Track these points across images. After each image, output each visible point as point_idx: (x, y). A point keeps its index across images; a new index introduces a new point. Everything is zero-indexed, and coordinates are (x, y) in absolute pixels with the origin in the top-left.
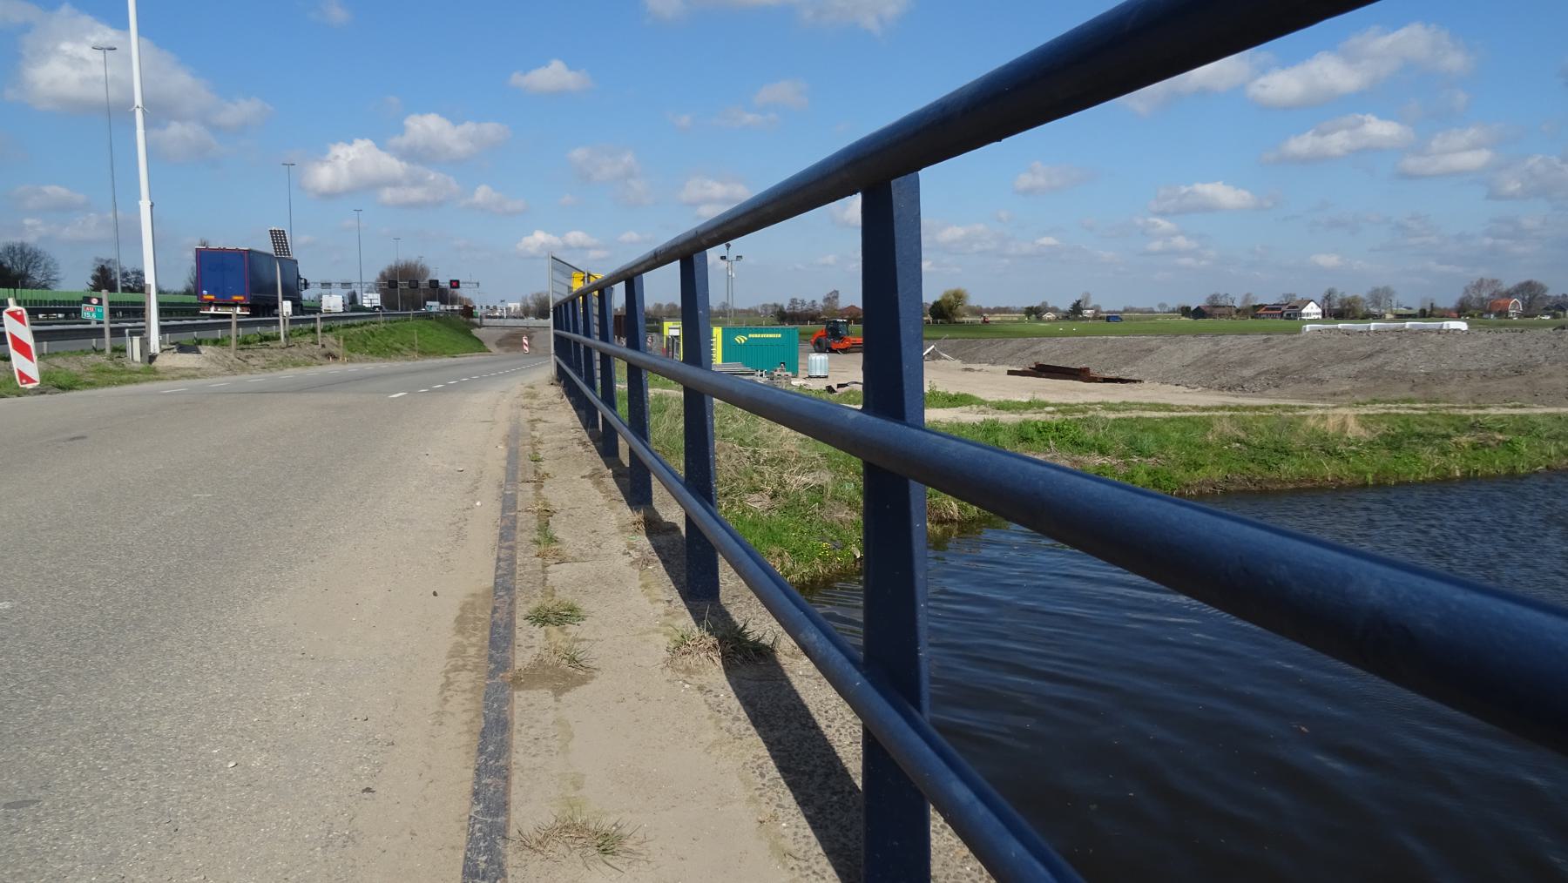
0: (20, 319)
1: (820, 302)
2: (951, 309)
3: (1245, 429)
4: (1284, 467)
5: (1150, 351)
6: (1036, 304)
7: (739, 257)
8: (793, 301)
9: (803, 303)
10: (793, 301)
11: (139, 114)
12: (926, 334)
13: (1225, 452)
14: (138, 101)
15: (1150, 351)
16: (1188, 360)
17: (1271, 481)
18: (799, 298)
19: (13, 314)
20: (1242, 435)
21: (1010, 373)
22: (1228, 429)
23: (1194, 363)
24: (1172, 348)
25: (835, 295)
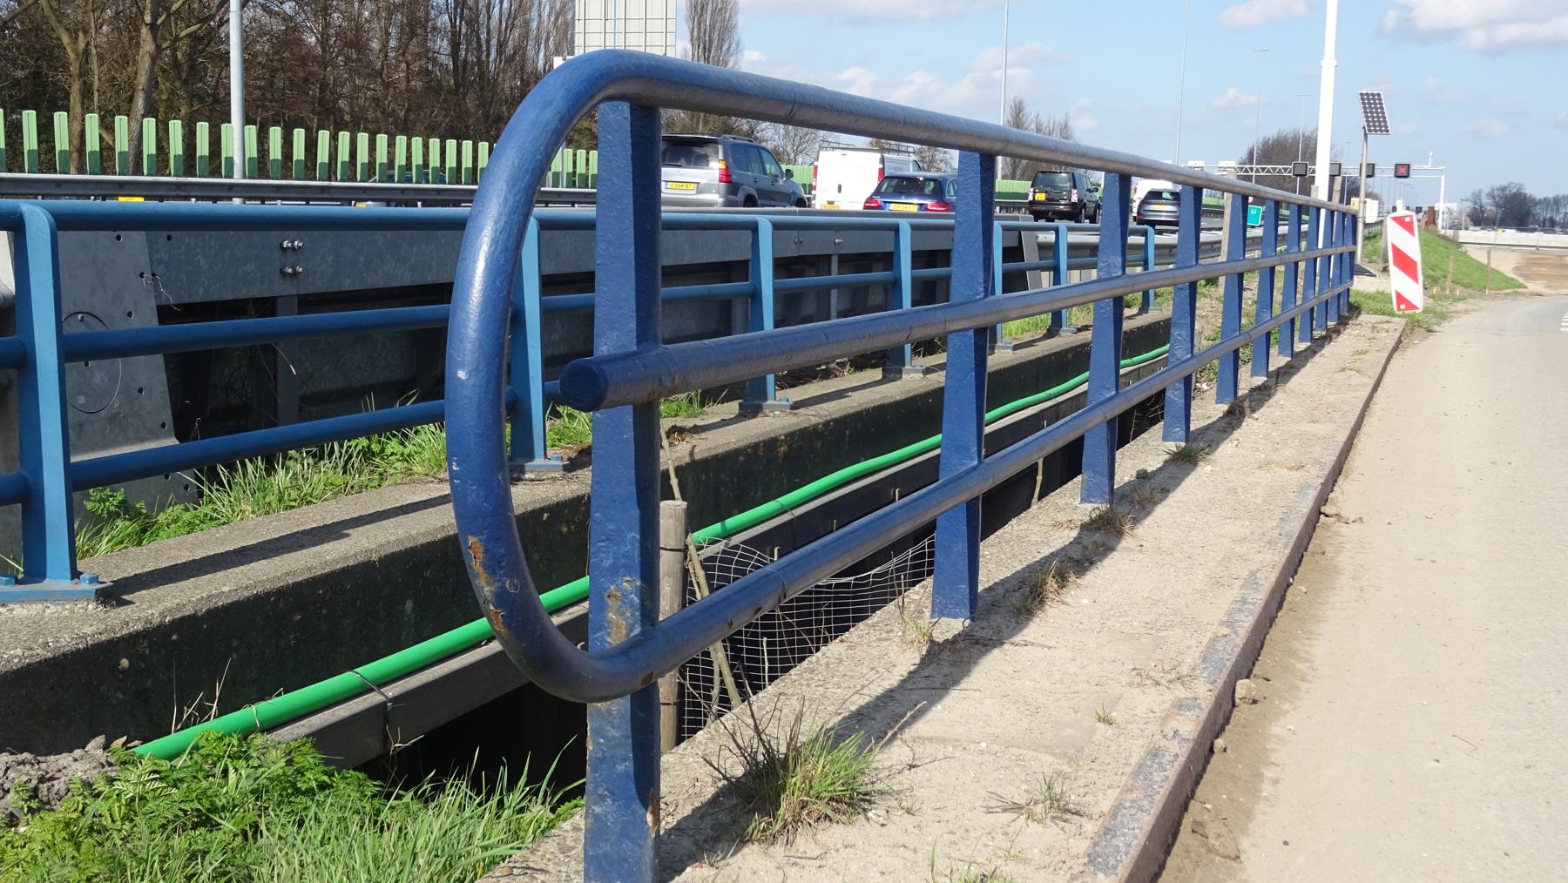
0: (1408, 227)
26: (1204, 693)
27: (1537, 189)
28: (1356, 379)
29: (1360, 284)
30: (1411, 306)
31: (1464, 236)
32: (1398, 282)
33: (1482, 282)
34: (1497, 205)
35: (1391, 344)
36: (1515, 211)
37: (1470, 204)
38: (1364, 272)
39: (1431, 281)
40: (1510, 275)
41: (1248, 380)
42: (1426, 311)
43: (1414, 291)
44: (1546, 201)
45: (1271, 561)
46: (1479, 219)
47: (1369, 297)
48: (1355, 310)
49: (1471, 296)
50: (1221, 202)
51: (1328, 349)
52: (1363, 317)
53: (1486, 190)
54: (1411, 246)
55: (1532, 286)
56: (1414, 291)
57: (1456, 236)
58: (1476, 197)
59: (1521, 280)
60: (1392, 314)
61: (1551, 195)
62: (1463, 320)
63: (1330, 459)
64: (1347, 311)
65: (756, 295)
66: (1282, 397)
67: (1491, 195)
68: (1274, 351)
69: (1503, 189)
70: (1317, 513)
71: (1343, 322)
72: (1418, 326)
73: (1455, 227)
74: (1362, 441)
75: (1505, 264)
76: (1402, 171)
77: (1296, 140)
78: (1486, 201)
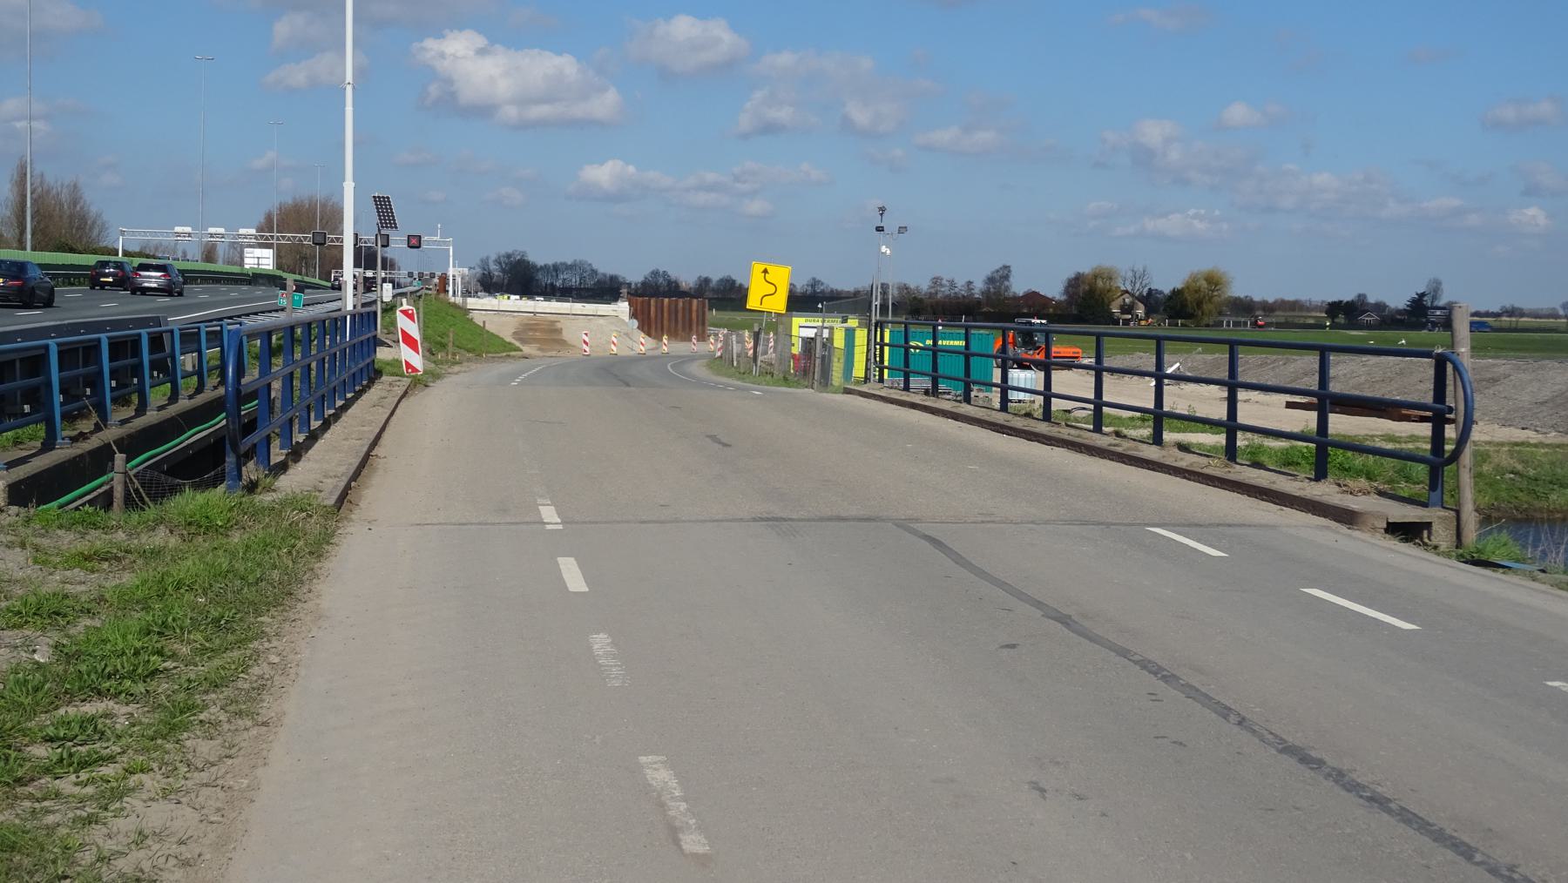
0: (411, 317)
1: (979, 286)
2: (1199, 304)
3: (1524, 462)
4: (1553, 497)
5: (1494, 381)
6: (1347, 296)
7: (902, 230)
8: (936, 281)
9: (952, 284)
10: (936, 281)
11: (349, 89)
12: (539, 501)
13: (1497, 482)
14: (349, 77)
15: (1494, 381)
16: (1546, 394)
17: (1541, 510)
18: (946, 277)
19: (405, 312)
20: (1519, 467)
21: (1290, 405)
22: (1505, 460)
23: (1553, 399)
24: (1525, 377)
25: (1004, 274)
26: (342, 484)
27: (540, 256)
28: (381, 410)
29: (382, 354)
30: (415, 370)
31: (472, 302)
32: (406, 354)
33: (483, 345)
34: (503, 271)
35: (400, 393)
36: (520, 278)
37: (479, 270)
38: (383, 344)
39: (430, 353)
40: (509, 339)
41: (315, 424)
42: (425, 372)
43: (417, 360)
44: (545, 268)
45: (356, 462)
46: (489, 285)
47: (388, 364)
48: (378, 373)
49: (469, 360)
50: (220, 261)
51: (364, 397)
52: (384, 378)
53: (493, 257)
54: (413, 330)
55: (526, 349)
56: (417, 360)
57: (465, 303)
58: (485, 262)
59: (518, 344)
60: (402, 375)
61: (550, 262)
62: (454, 378)
63: (372, 437)
64: (374, 374)
65: (49, 384)
66: (346, 418)
67: (498, 262)
68: (296, 427)
69: (509, 256)
70: (367, 456)
71: (372, 382)
72: (418, 383)
73: (467, 293)
74: (385, 435)
75: (506, 331)
76: (414, 242)
77: (312, 208)
78: (493, 267)
